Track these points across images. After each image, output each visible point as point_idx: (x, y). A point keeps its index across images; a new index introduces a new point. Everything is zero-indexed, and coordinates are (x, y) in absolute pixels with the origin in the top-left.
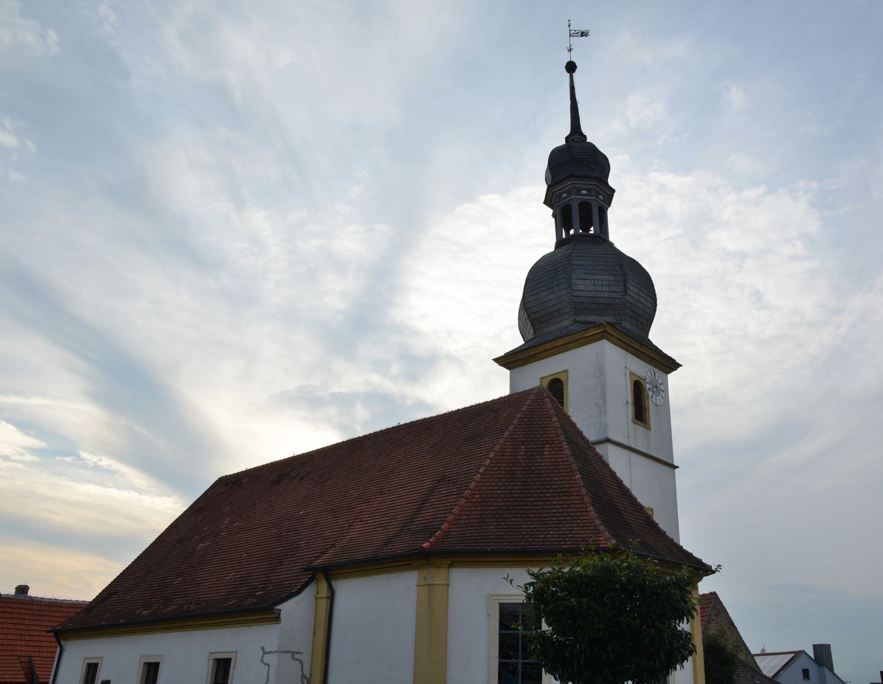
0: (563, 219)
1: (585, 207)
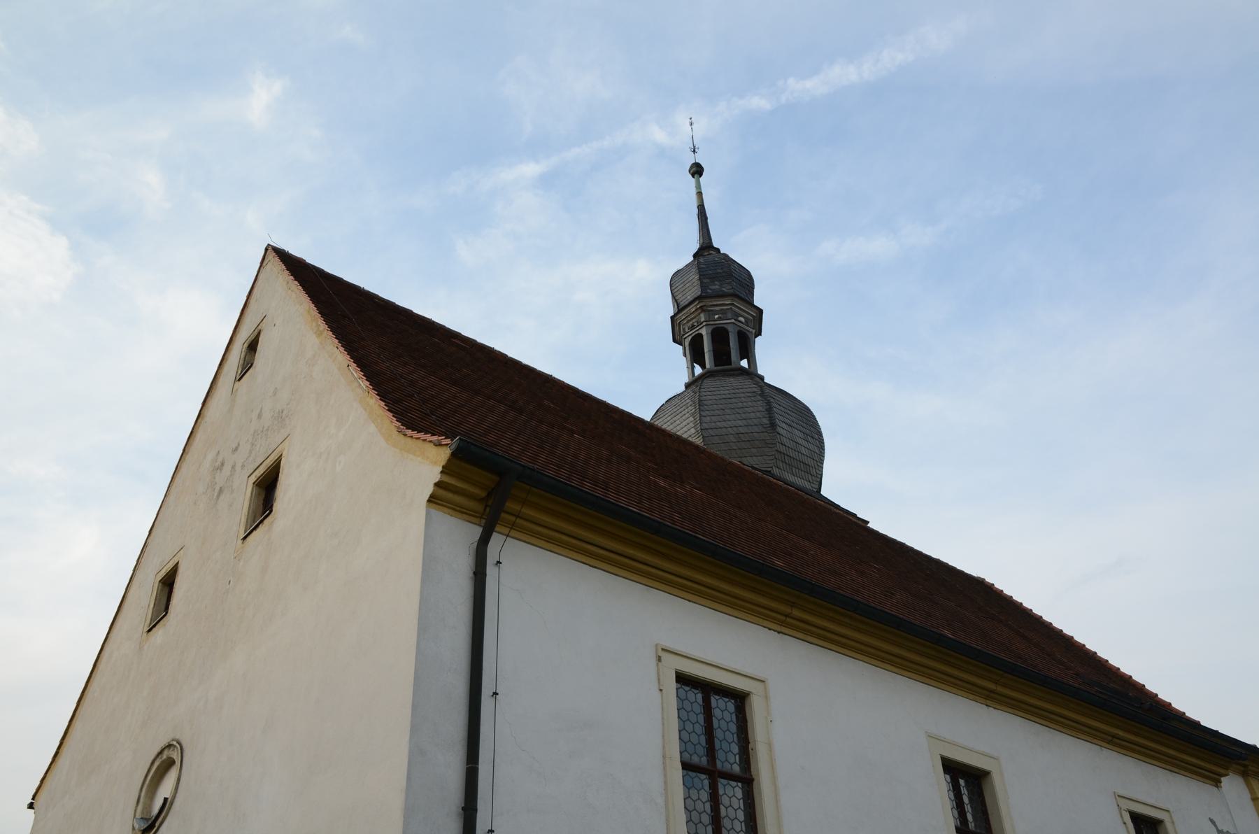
0: (696, 355)
1: (720, 336)
